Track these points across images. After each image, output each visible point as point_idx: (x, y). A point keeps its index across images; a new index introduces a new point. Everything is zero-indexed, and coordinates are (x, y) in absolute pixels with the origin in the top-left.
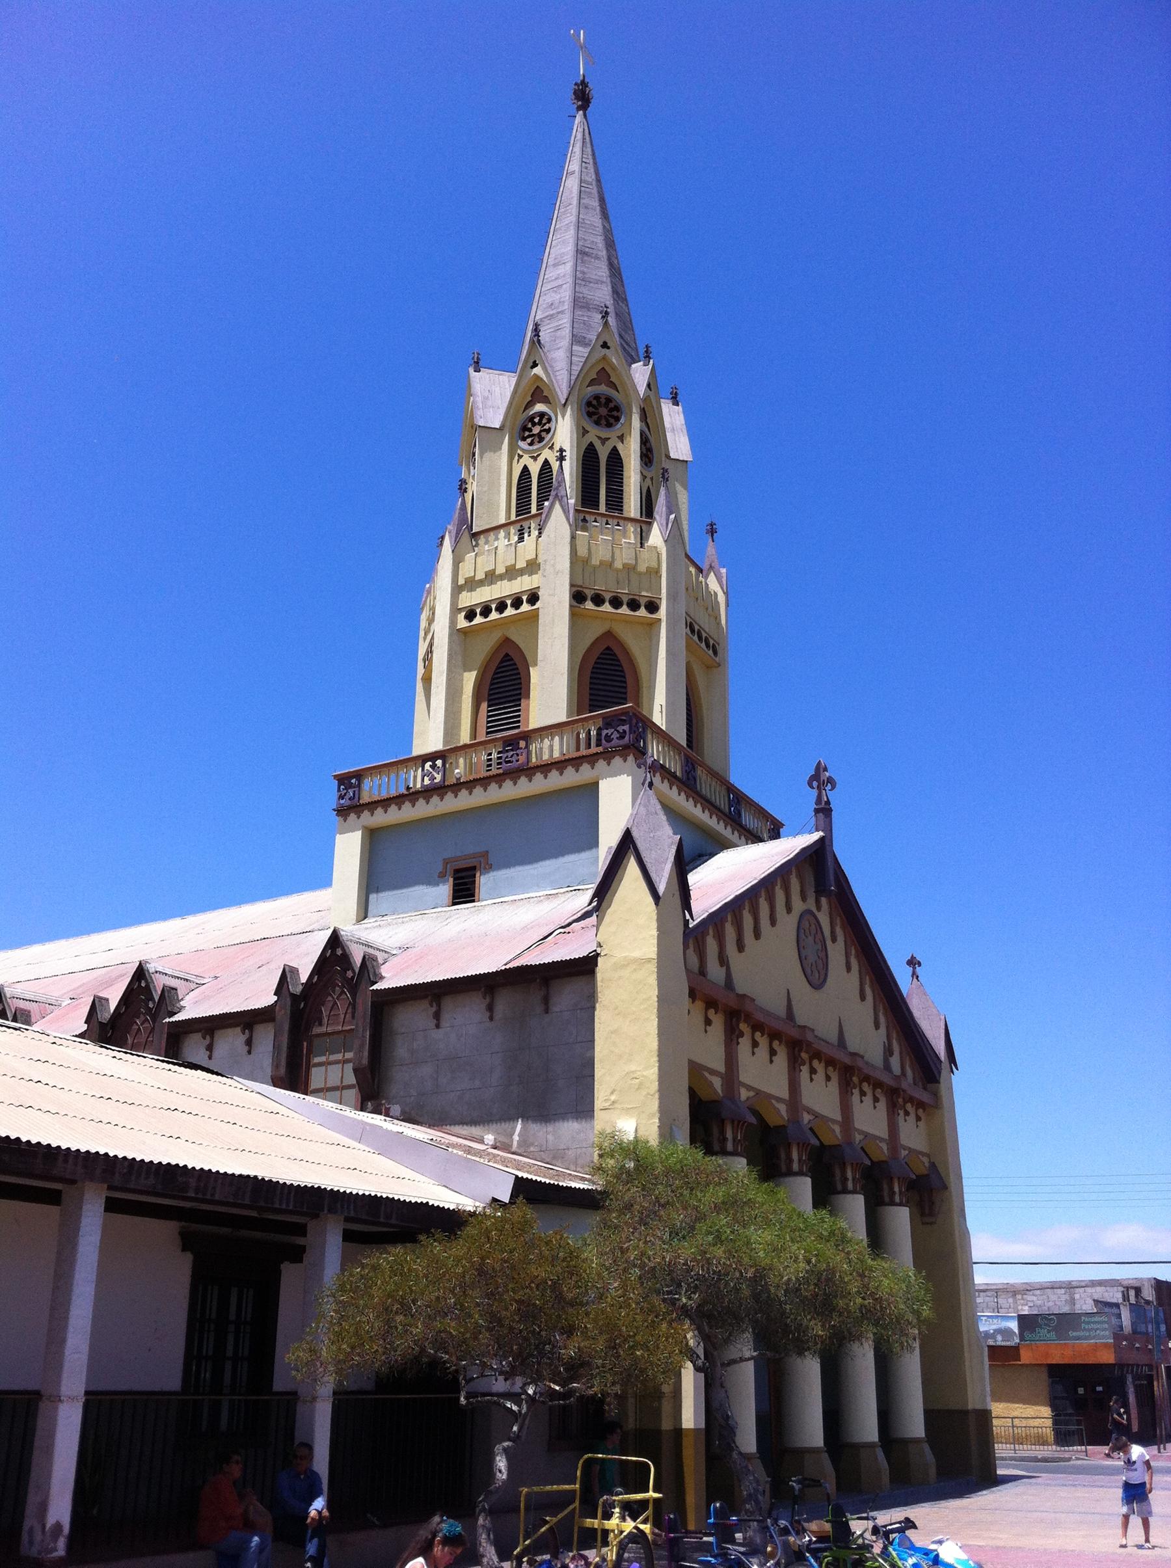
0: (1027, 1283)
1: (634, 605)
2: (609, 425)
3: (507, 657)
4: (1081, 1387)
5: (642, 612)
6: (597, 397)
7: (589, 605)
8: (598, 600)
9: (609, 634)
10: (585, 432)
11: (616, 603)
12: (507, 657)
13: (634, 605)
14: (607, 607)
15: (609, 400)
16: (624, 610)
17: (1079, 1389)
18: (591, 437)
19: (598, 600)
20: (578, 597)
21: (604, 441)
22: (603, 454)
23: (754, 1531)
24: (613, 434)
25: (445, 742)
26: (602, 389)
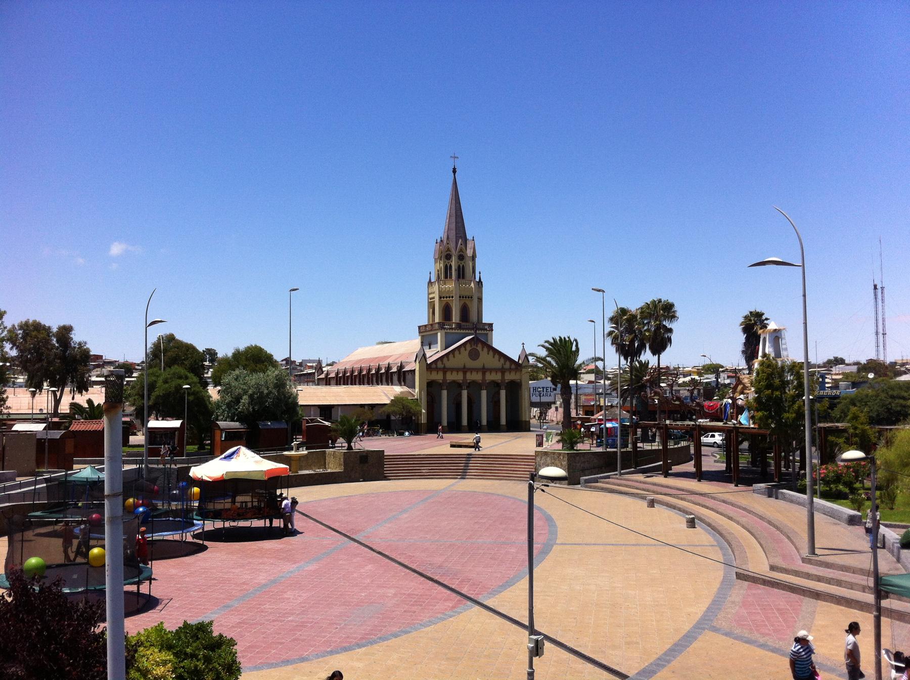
0: (512, 585)
1: (449, 297)
2: (447, 260)
3: (447, 305)
4: (639, 428)
5: (451, 298)
6: (447, 254)
7: (442, 299)
8: (444, 298)
9: (447, 302)
10: (458, 262)
11: (447, 298)
12: (447, 305)
13: (449, 297)
14: (445, 299)
15: (462, 255)
16: (448, 299)
17: (638, 430)
18: (459, 263)
19: (444, 298)
20: (440, 298)
21: (448, 263)
22: (461, 266)
23: (200, 655)
24: (450, 261)
25: (428, 323)
26: (448, 253)
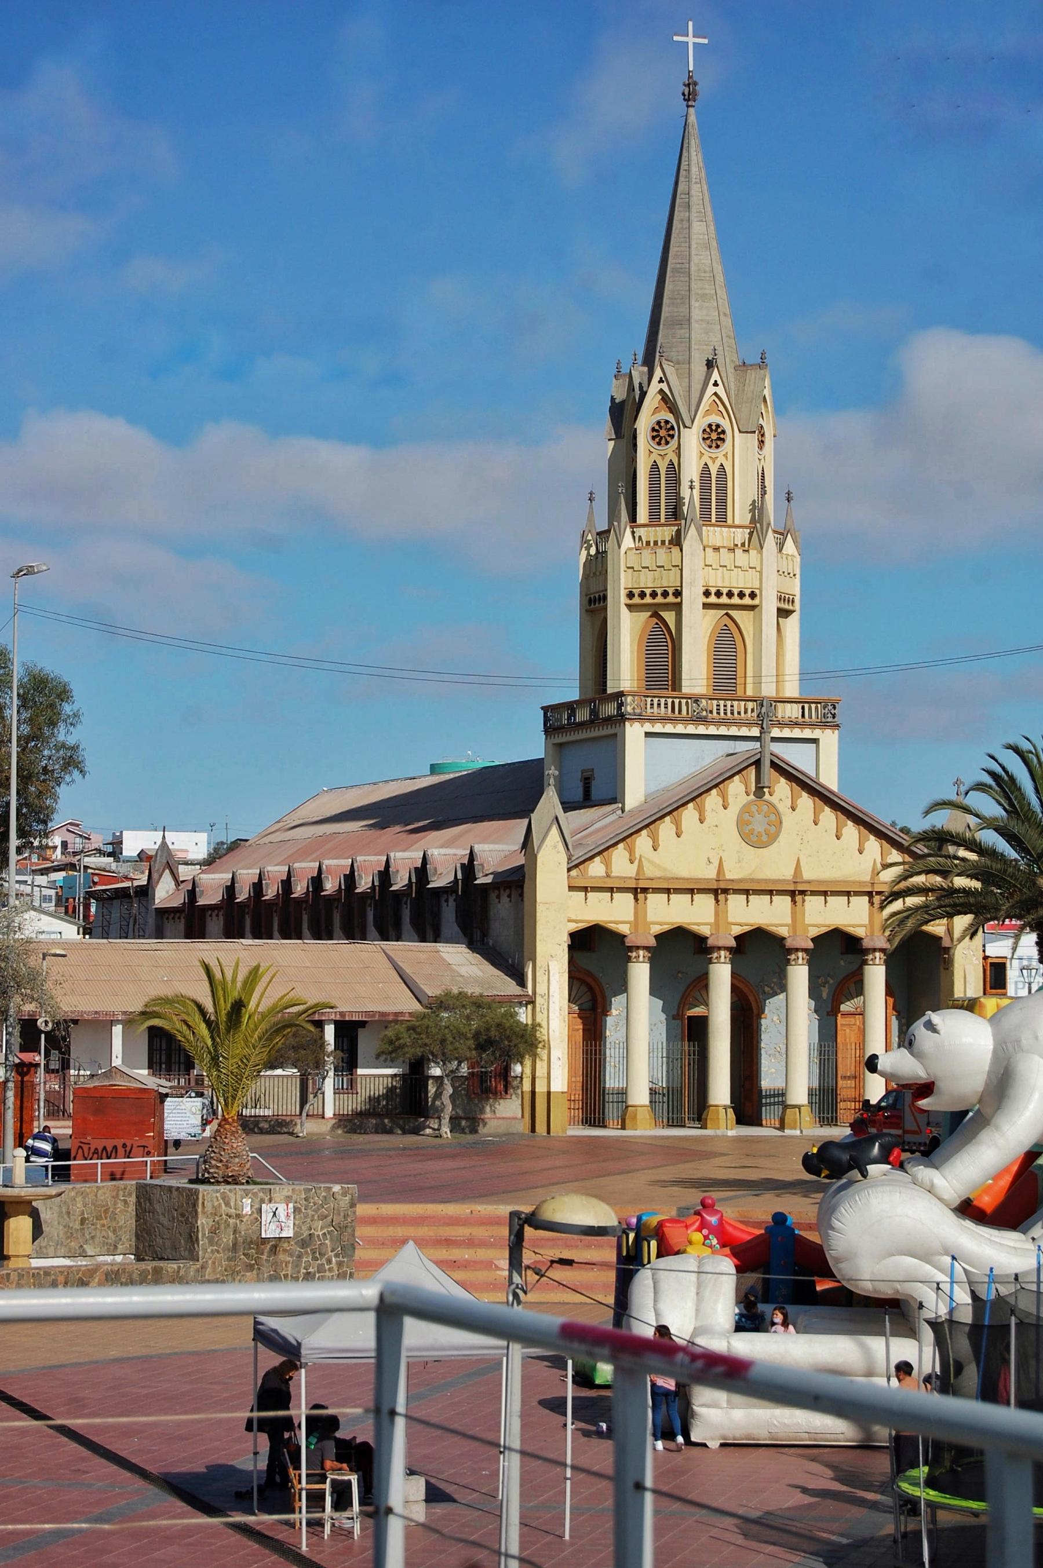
18: (706, 459)
